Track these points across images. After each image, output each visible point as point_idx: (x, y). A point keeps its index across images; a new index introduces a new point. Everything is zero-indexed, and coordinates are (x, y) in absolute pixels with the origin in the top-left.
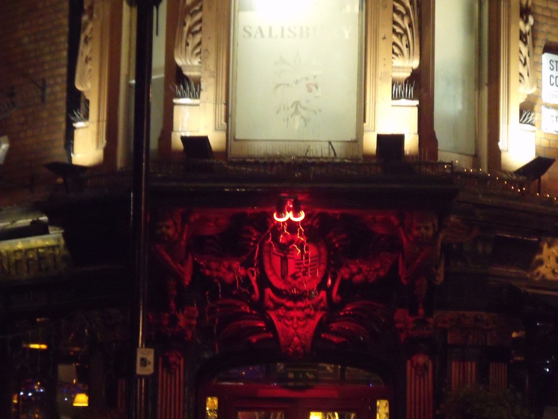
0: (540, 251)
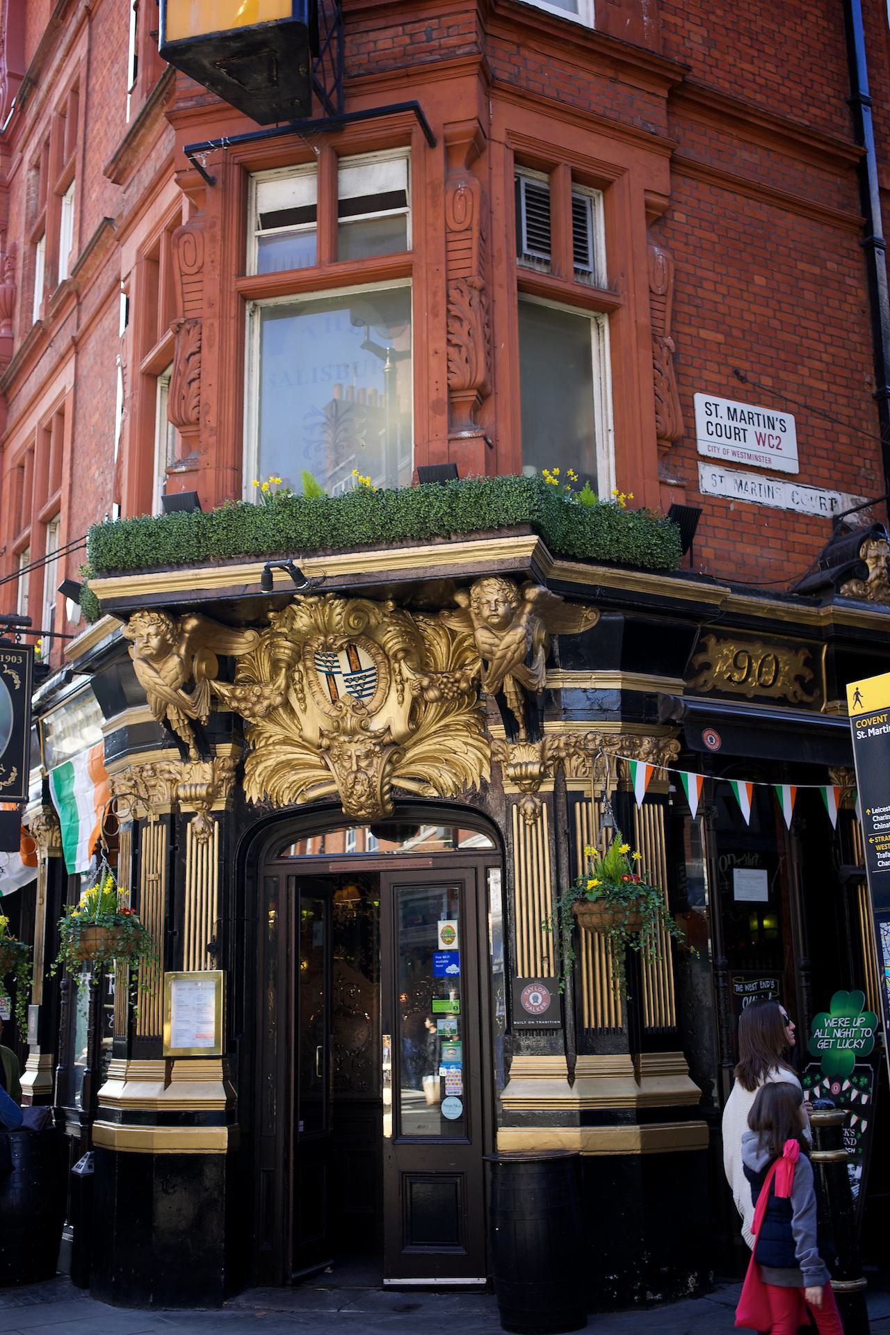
0: (703, 648)
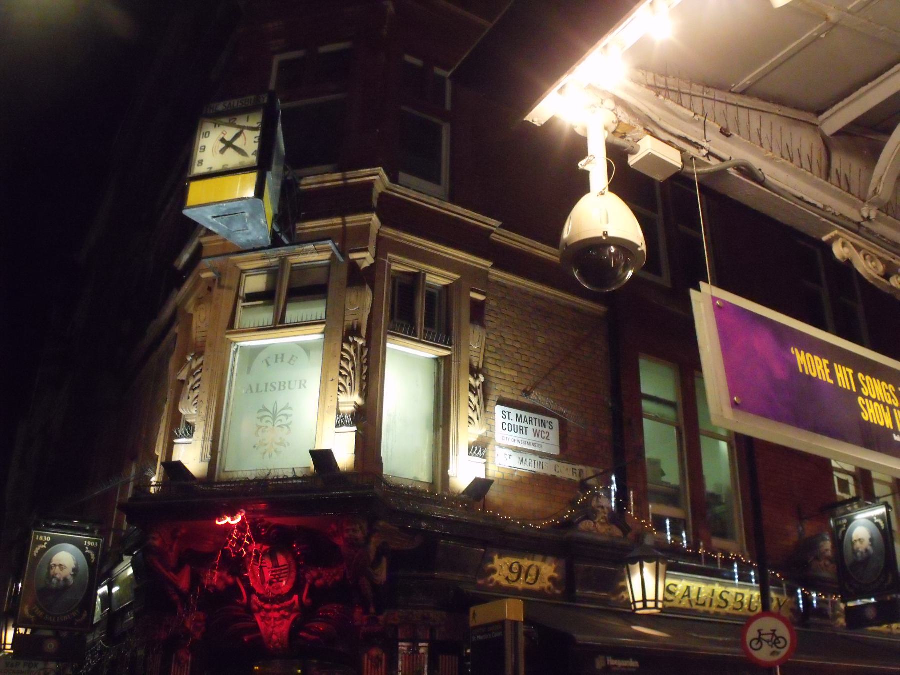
0: (492, 561)
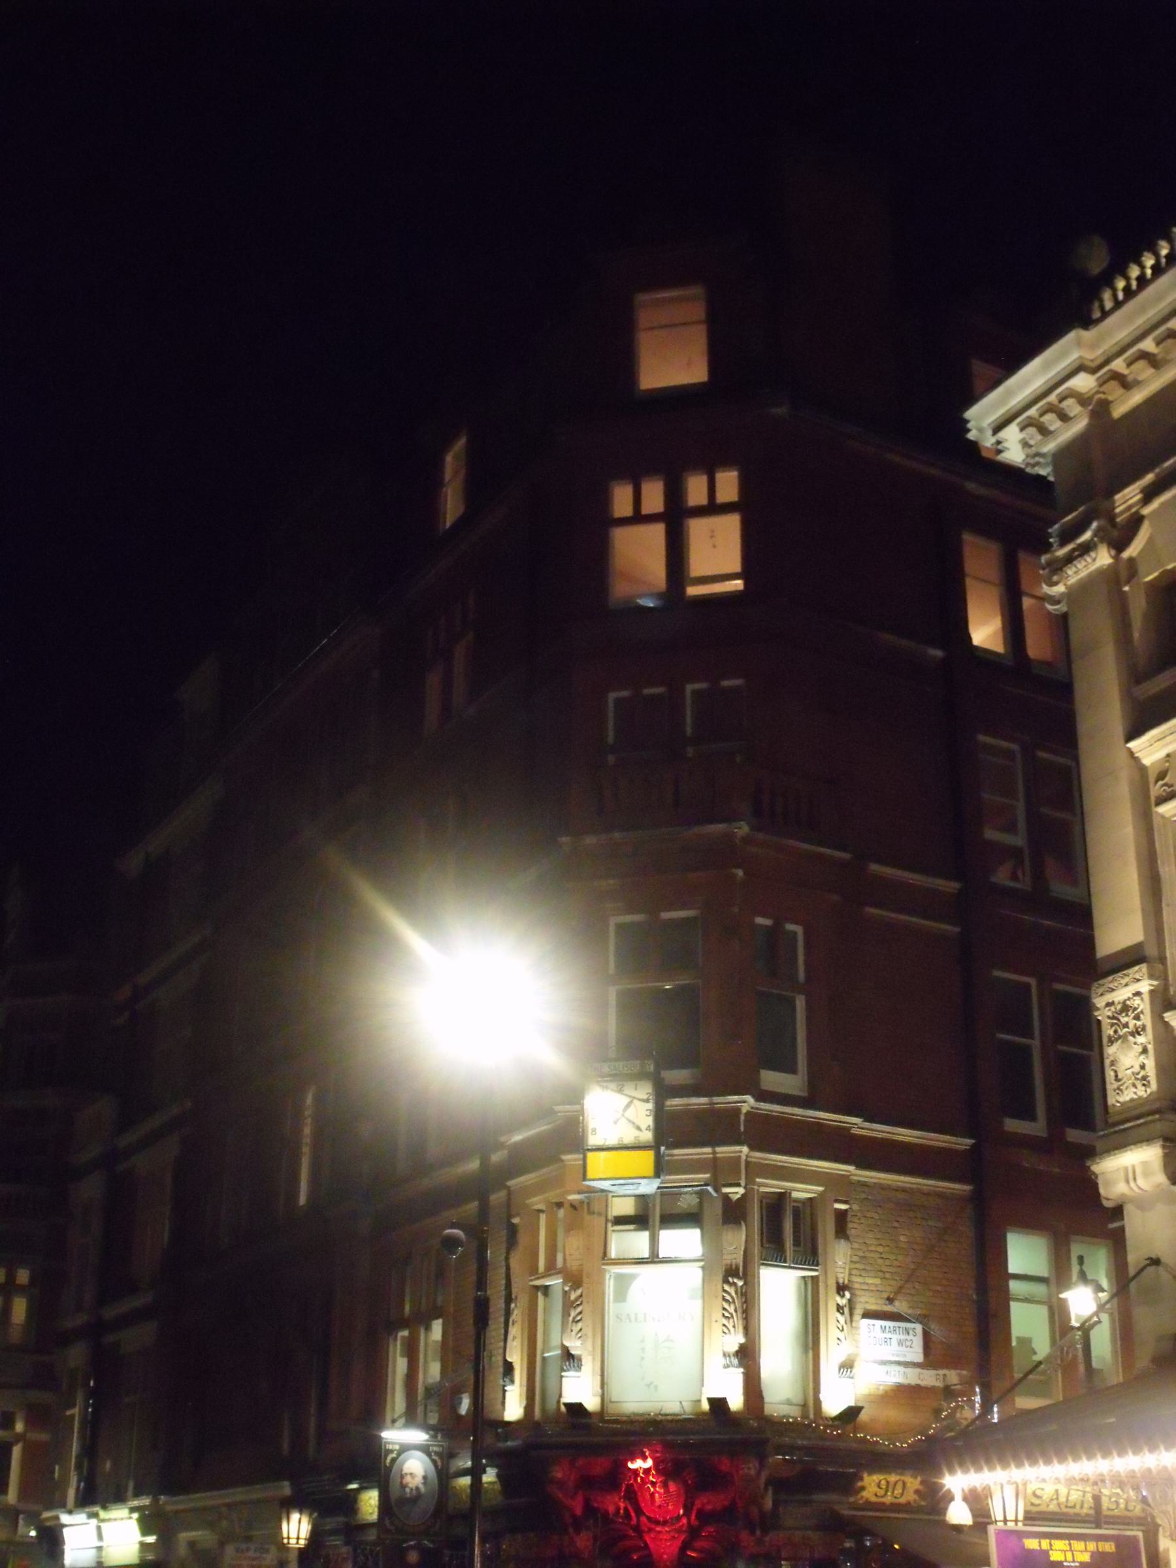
0: (862, 1479)
